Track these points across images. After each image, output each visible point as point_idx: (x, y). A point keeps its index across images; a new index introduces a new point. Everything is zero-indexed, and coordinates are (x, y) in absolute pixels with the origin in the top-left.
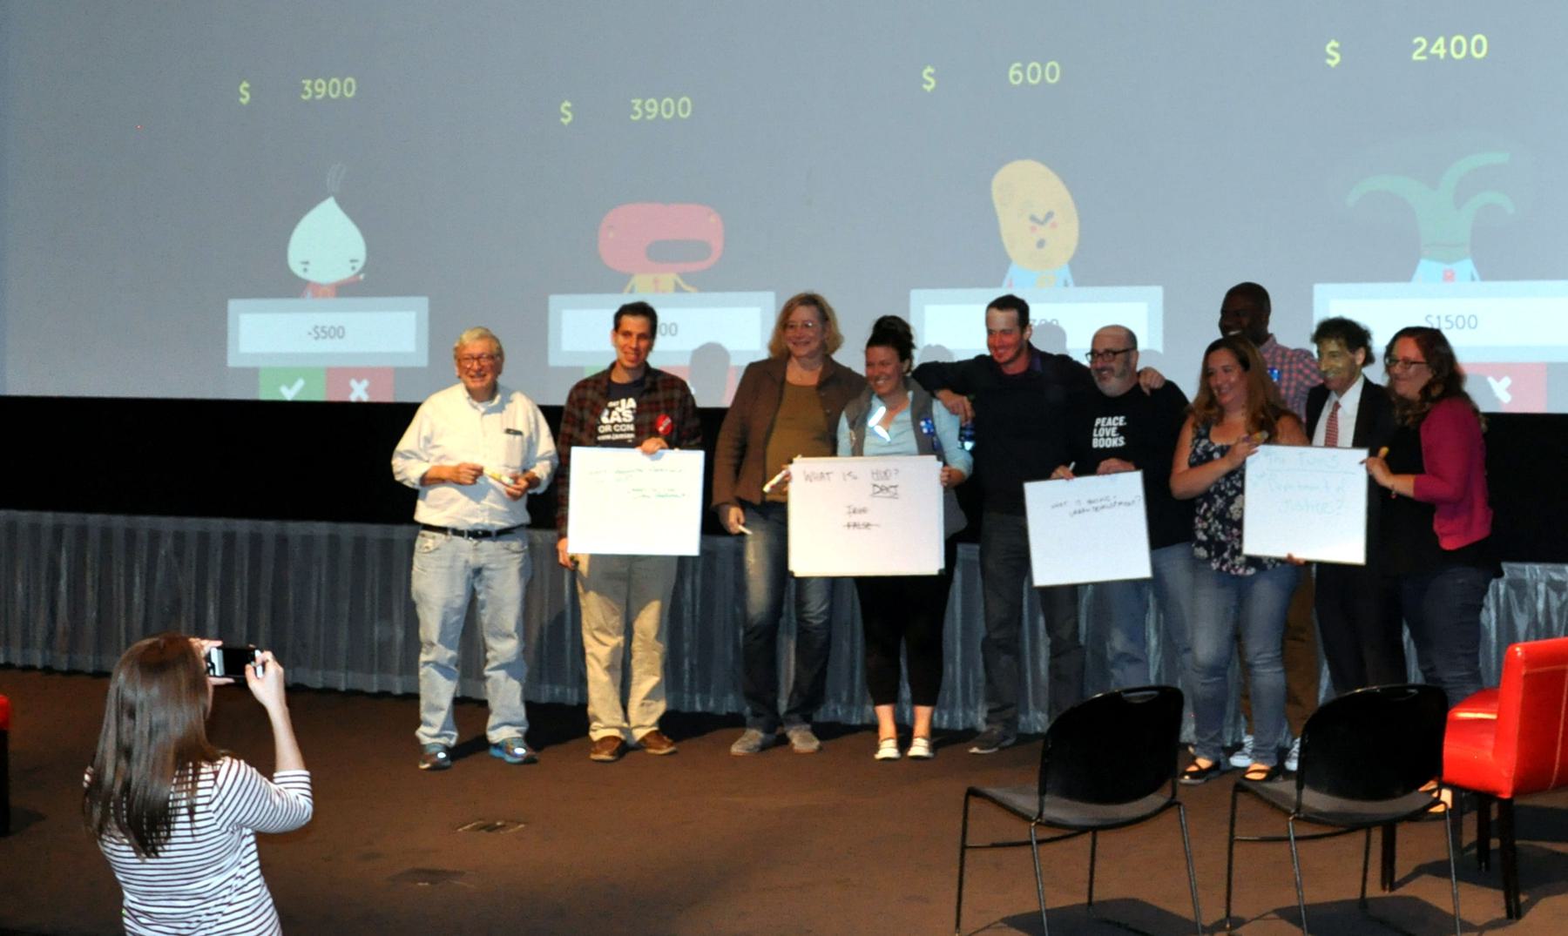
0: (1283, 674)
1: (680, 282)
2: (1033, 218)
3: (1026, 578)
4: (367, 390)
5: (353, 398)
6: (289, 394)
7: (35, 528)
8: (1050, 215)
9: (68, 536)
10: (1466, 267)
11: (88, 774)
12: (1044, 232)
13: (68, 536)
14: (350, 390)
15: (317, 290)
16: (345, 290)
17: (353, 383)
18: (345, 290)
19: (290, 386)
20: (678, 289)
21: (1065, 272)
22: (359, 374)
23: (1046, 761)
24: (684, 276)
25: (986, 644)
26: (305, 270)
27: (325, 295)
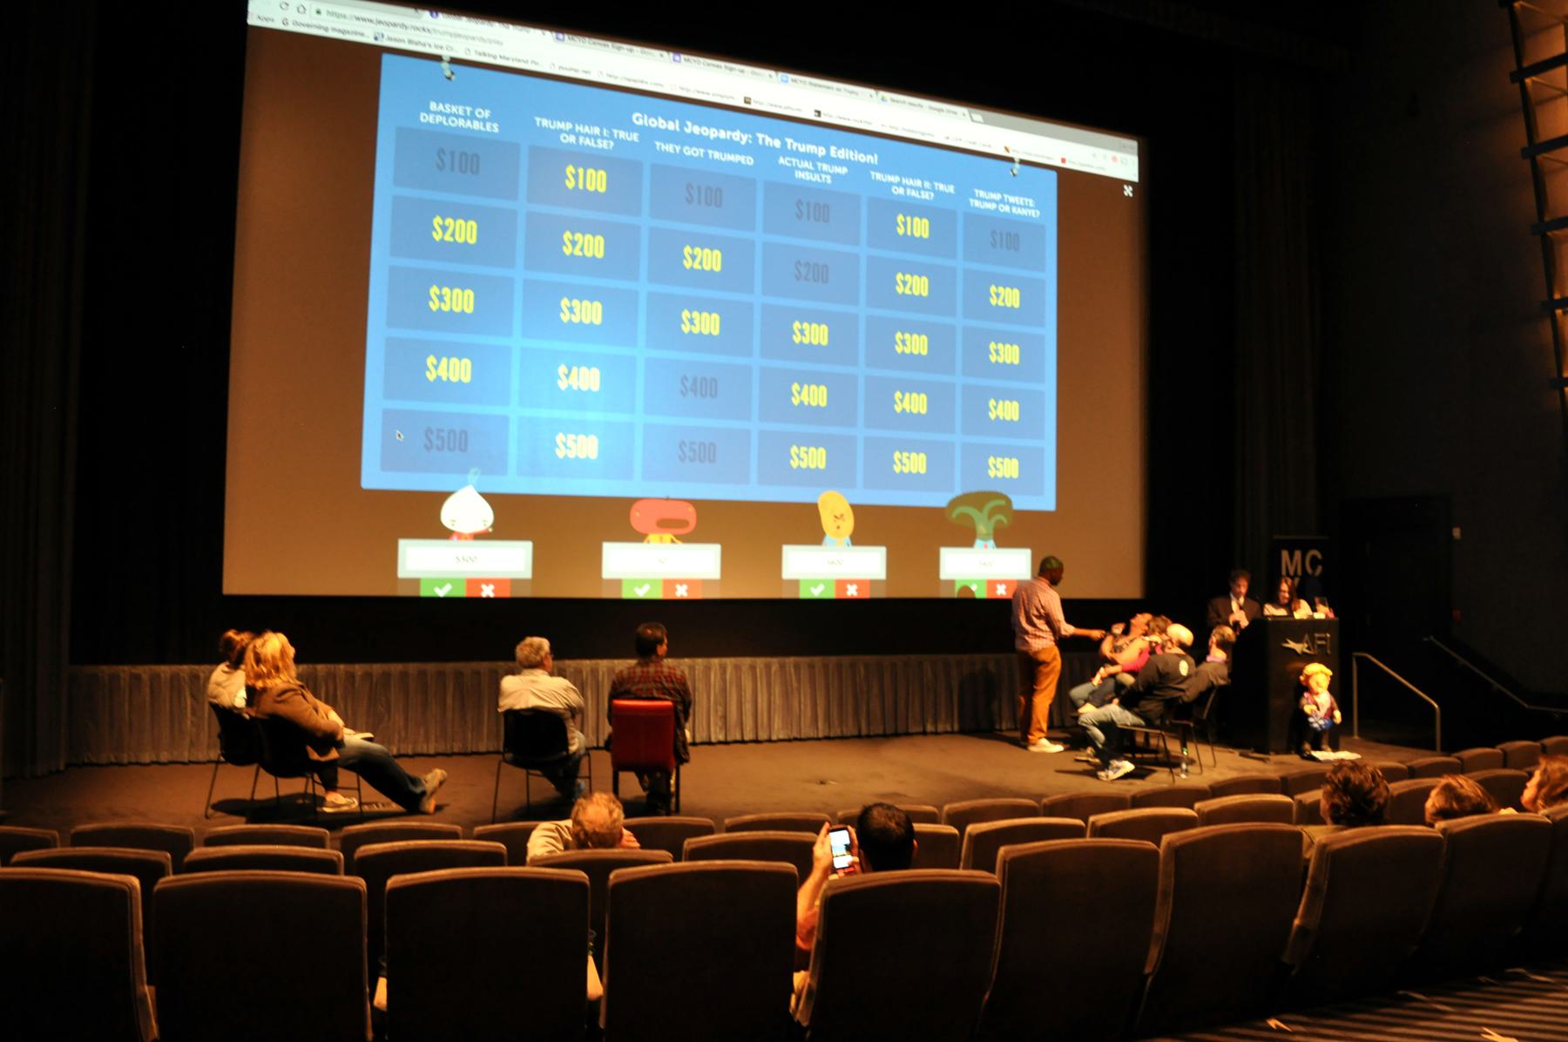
0: (579, 775)
1: (674, 538)
2: (836, 517)
3: (522, 713)
4: (494, 591)
5: (484, 595)
6: (441, 592)
7: (422, 674)
8: (842, 516)
9: (745, 668)
10: (991, 543)
11: (591, 941)
12: (839, 522)
13: (745, 668)
14: (481, 590)
15: (460, 536)
16: (479, 536)
17: (484, 587)
18: (479, 536)
19: (441, 588)
20: (673, 541)
21: (847, 539)
22: (488, 582)
23: (590, 844)
24: (676, 536)
25: (1448, 749)
26: (453, 525)
27: (466, 538)
